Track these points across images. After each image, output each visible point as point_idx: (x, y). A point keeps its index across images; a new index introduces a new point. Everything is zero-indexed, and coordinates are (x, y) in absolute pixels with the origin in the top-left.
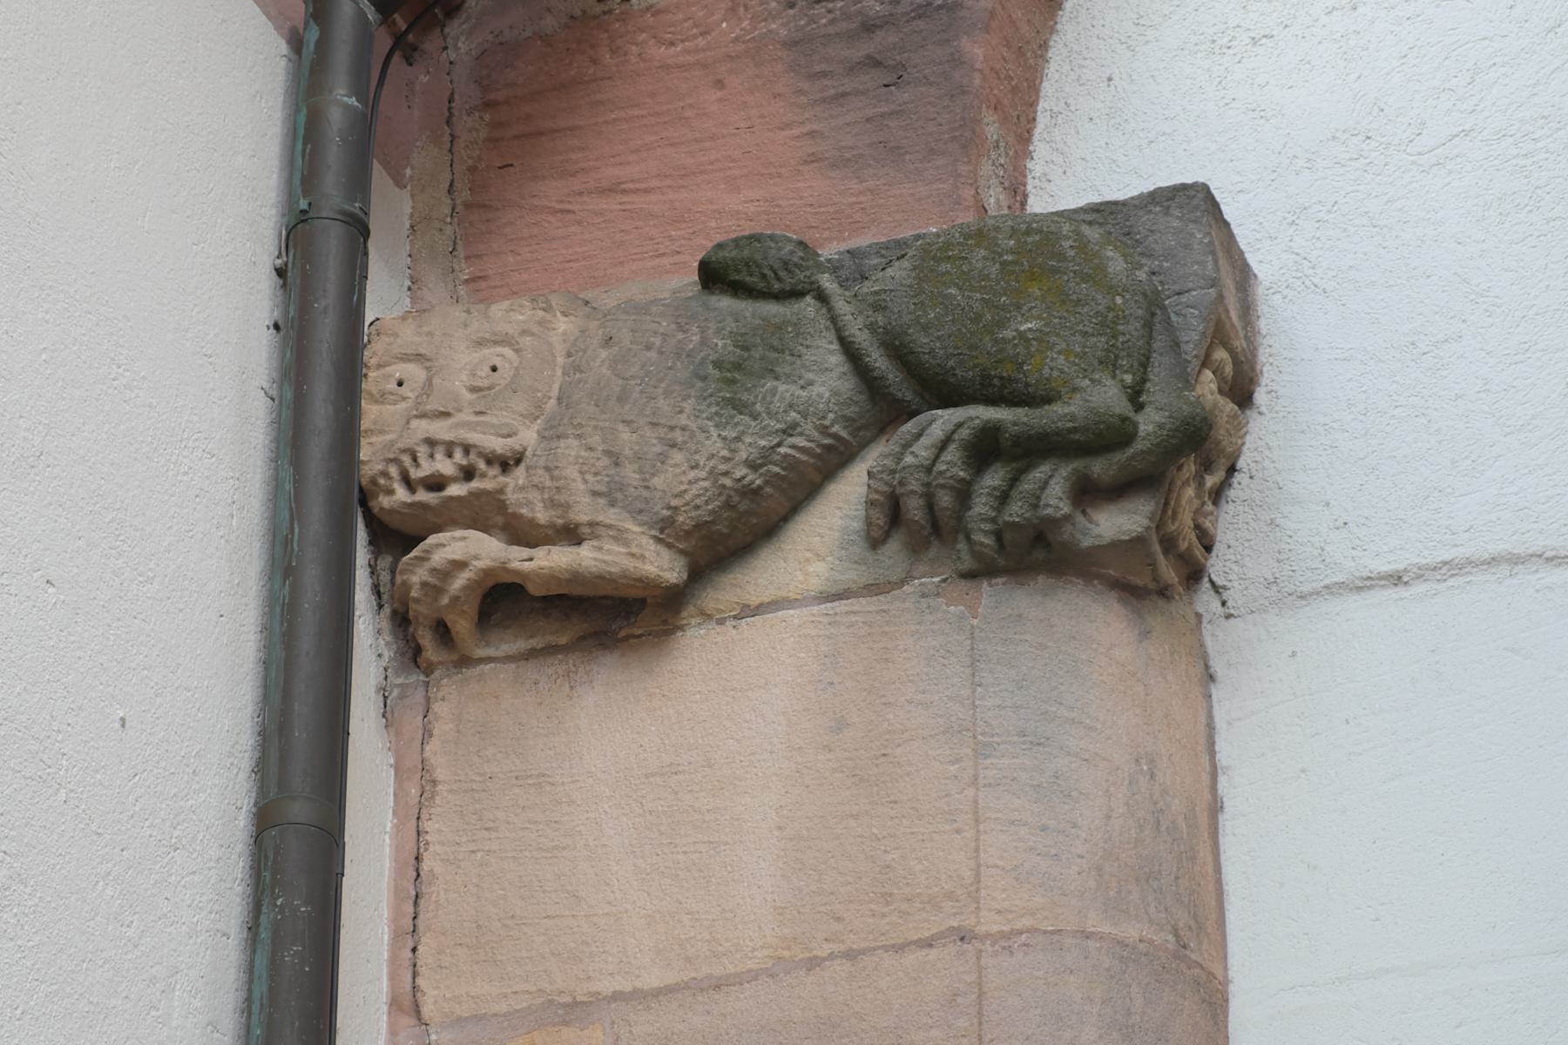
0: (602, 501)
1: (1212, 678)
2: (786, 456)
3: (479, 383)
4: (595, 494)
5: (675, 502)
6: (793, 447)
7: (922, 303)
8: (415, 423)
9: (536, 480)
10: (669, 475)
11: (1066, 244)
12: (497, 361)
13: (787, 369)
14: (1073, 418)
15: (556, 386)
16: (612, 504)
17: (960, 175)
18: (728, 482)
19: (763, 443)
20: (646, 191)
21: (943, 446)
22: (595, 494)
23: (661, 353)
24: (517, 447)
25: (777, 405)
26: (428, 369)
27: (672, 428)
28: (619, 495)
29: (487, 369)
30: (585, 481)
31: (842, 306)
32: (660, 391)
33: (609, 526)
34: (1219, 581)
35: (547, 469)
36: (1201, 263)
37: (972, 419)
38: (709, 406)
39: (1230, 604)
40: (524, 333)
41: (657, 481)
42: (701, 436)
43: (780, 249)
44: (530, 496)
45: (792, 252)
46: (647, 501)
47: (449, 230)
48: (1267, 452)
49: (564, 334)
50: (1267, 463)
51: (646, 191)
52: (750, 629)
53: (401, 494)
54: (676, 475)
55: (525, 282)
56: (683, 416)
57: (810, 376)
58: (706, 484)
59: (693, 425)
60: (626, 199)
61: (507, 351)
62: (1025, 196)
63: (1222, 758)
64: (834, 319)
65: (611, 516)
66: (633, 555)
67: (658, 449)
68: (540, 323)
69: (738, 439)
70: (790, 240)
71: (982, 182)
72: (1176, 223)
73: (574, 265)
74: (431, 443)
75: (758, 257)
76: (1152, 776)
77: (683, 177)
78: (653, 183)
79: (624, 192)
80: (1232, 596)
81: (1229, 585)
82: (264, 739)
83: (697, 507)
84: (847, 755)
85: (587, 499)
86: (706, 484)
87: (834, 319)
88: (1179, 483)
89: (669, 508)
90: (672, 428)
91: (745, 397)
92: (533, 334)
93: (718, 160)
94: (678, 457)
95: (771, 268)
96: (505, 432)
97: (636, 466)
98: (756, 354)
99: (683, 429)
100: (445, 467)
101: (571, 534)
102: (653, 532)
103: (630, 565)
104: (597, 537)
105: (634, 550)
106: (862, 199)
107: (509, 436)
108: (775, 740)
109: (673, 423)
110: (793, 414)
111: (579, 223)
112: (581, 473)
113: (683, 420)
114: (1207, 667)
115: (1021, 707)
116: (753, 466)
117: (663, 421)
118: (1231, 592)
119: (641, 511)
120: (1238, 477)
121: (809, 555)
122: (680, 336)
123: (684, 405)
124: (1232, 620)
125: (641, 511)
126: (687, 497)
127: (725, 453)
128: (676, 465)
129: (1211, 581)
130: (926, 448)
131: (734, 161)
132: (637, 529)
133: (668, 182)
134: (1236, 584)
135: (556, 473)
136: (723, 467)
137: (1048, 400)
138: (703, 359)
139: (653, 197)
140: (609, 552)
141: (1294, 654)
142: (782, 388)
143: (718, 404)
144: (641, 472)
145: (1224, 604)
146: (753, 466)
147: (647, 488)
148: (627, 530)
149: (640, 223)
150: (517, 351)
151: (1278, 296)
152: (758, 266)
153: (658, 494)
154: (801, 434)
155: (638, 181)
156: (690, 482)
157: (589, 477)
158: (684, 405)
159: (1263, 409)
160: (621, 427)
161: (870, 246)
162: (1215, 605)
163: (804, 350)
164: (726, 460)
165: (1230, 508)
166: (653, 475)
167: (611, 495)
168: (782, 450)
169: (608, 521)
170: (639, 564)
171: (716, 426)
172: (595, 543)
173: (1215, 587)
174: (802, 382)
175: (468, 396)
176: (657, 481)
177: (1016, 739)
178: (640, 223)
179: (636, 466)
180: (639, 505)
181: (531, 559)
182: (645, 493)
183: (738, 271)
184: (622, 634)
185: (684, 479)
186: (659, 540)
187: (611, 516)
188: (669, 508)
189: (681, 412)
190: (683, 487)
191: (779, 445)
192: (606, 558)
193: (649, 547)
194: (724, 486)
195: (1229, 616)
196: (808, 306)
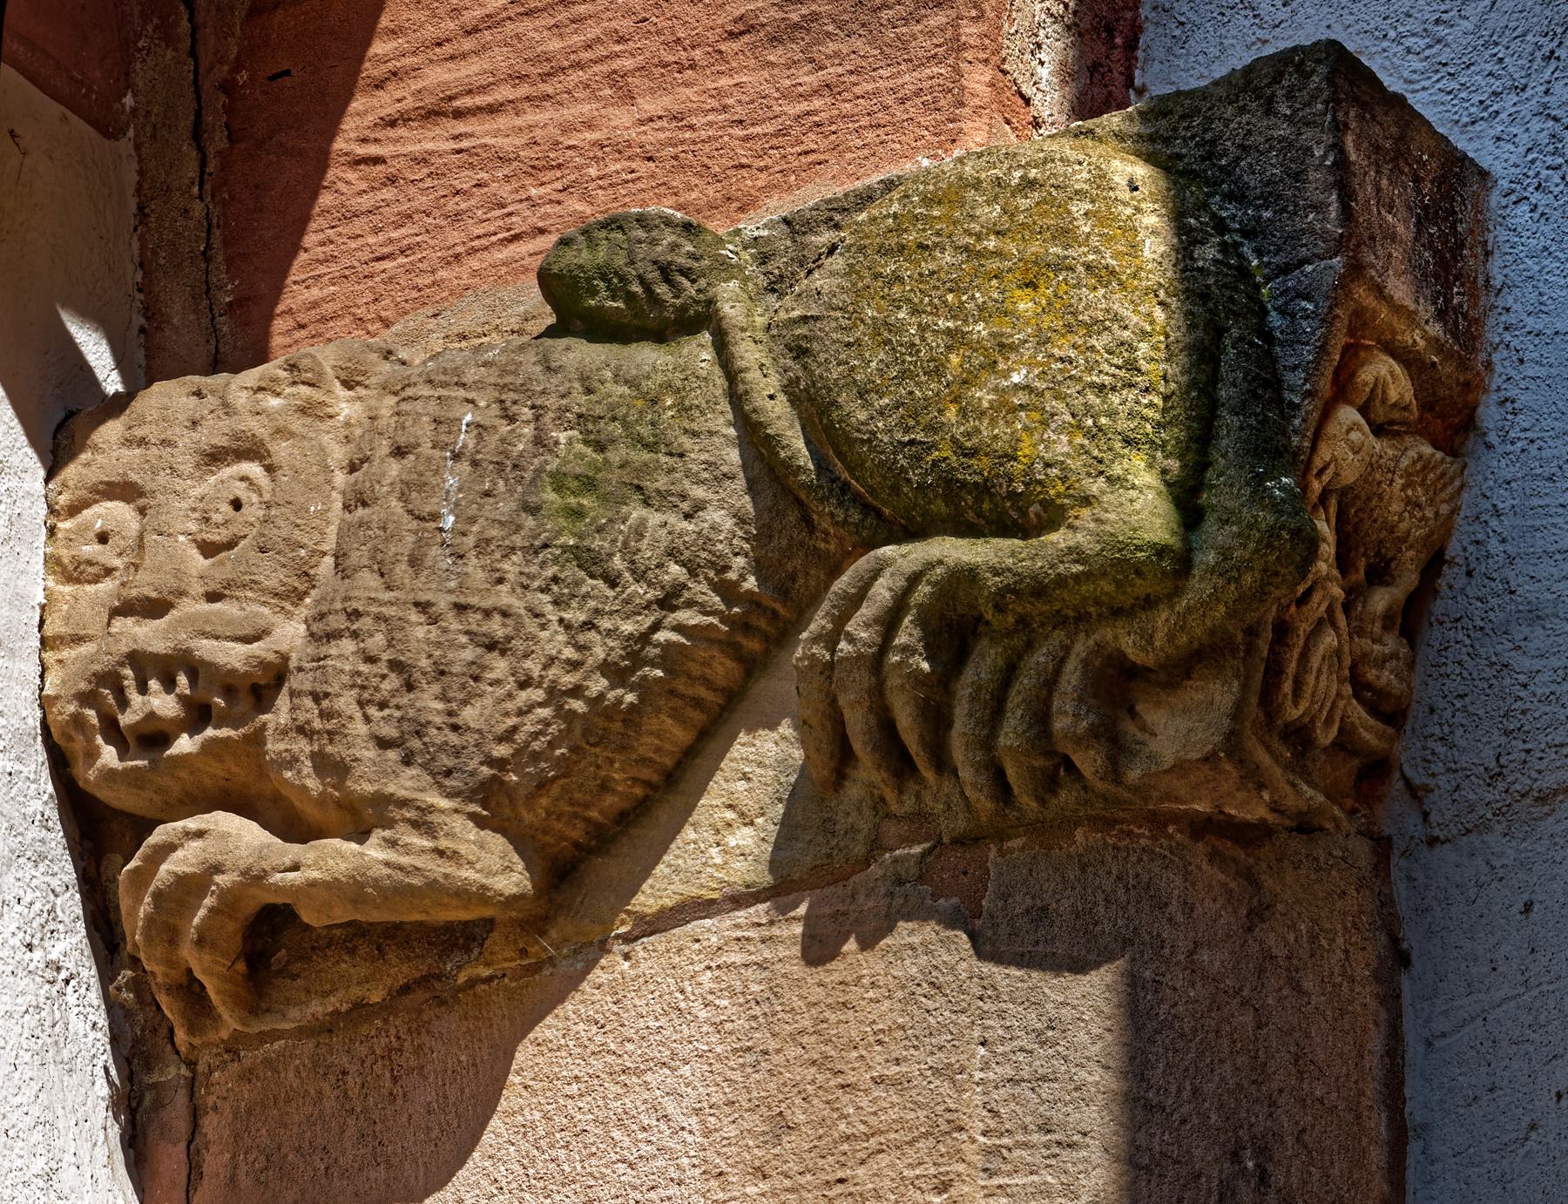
0: (393, 755)
1: (1404, 960)
2: (668, 646)
3: (215, 536)
4: (383, 744)
5: (502, 751)
6: (679, 628)
7: (858, 342)
8: (119, 624)
9: (302, 717)
10: (488, 701)
11: (1078, 208)
12: (240, 490)
13: (662, 482)
14: (1077, 554)
15: (332, 531)
16: (407, 761)
17: (964, 47)
18: (578, 705)
19: (628, 627)
20: (493, 109)
21: (889, 622)
22: (383, 744)
23: (475, 463)
24: (271, 657)
25: (647, 554)
26: (142, 511)
27: (487, 613)
28: (415, 744)
29: (226, 508)
30: (367, 719)
31: (749, 354)
32: (470, 541)
33: (404, 803)
34: (1418, 778)
35: (317, 698)
36: (1319, 208)
37: (930, 566)
38: (543, 565)
39: (1434, 818)
40: (281, 432)
41: (469, 715)
42: (531, 626)
43: (654, 242)
44: (295, 747)
45: (674, 247)
46: (457, 752)
47: (198, 209)
48: (1494, 523)
49: (348, 424)
50: (1494, 545)
51: (493, 109)
52: (650, 955)
53: (109, 755)
54: (500, 701)
55: (315, 305)
56: (504, 588)
57: (699, 492)
58: (544, 712)
59: (517, 604)
60: (461, 127)
61: (253, 469)
62: (1136, 30)
63: (1414, 1111)
64: (732, 374)
65: (406, 783)
66: (441, 853)
67: (469, 654)
68: (303, 411)
69: (589, 625)
70: (668, 222)
71: (1012, 47)
72: (1284, 130)
73: (387, 264)
74: (137, 659)
75: (620, 261)
76: (1263, 1177)
77: (545, 77)
78: (504, 93)
79: (459, 114)
80: (1442, 807)
81: (1431, 782)
82: (132, 1113)
83: (536, 757)
84: (787, 1183)
85: (370, 753)
86: (544, 712)
87: (732, 374)
88: (1304, 628)
89: (490, 761)
90: (487, 613)
91: (597, 543)
92: (292, 435)
93: (598, 40)
94: (500, 666)
95: (642, 280)
96: (248, 631)
97: (436, 688)
98: (615, 456)
99: (505, 614)
100: (164, 704)
101: (358, 819)
102: (474, 808)
103: (438, 869)
104: (389, 824)
105: (443, 843)
106: (817, 103)
107: (257, 638)
108: (685, 1161)
109: (487, 603)
110: (675, 569)
111: (392, 180)
112: (361, 704)
113: (504, 596)
114: (1395, 941)
115: (1044, 1079)
116: (615, 673)
117: (474, 600)
118: (1434, 797)
119: (449, 773)
120: (1450, 576)
121: (730, 815)
122: (505, 429)
123: (506, 566)
124: (1438, 850)
125: (449, 773)
126: (520, 737)
127: (569, 653)
128: (496, 683)
129: (1408, 783)
130: (867, 625)
131: (621, 40)
132: (444, 803)
133: (524, 90)
134: (1442, 781)
135: (325, 703)
136: (568, 680)
137: (1053, 517)
138: (539, 471)
139: (502, 122)
140: (408, 849)
141: (1528, 907)
142: (655, 518)
143: (556, 560)
144: (443, 697)
145: (1426, 815)
146: (615, 673)
147: (455, 728)
148: (431, 809)
149: (483, 175)
150: (270, 469)
151: (1525, 207)
152: (622, 279)
153: (471, 738)
154: (690, 604)
155: (483, 89)
156: (521, 713)
157: (373, 711)
158: (506, 566)
159: (1493, 438)
160: (414, 617)
161: (816, 208)
162: (1413, 823)
163: (687, 442)
164: (574, 665)
165: (1435, 635)
166: (465, 702)
167: (403, 744)
168: (661, 636)
169: (402, 793)
170: (448, 868)
171: (556, 603)
172: (387, 833)
173: (1415, 792)
174: (685, 506)
175: (199, 562)
176: (469, 715)
177: (1036, 1138)
178: (483, 175)
179: (436, 688)
180: (446, 761)
181: (295, 867)
182: (454, 739)
183: (594, 292)
184: (462, 978)
185: (509, 706)
186: (480, 822)
187: (406, 783)
188: (490, 761)
189: (500, 581)
190: (511, 721)
191: (656, 627)
192: (405, 860)
193: (464, 834)
194: (573, 712)
195: (1433, 841)
196: (699, 351)
